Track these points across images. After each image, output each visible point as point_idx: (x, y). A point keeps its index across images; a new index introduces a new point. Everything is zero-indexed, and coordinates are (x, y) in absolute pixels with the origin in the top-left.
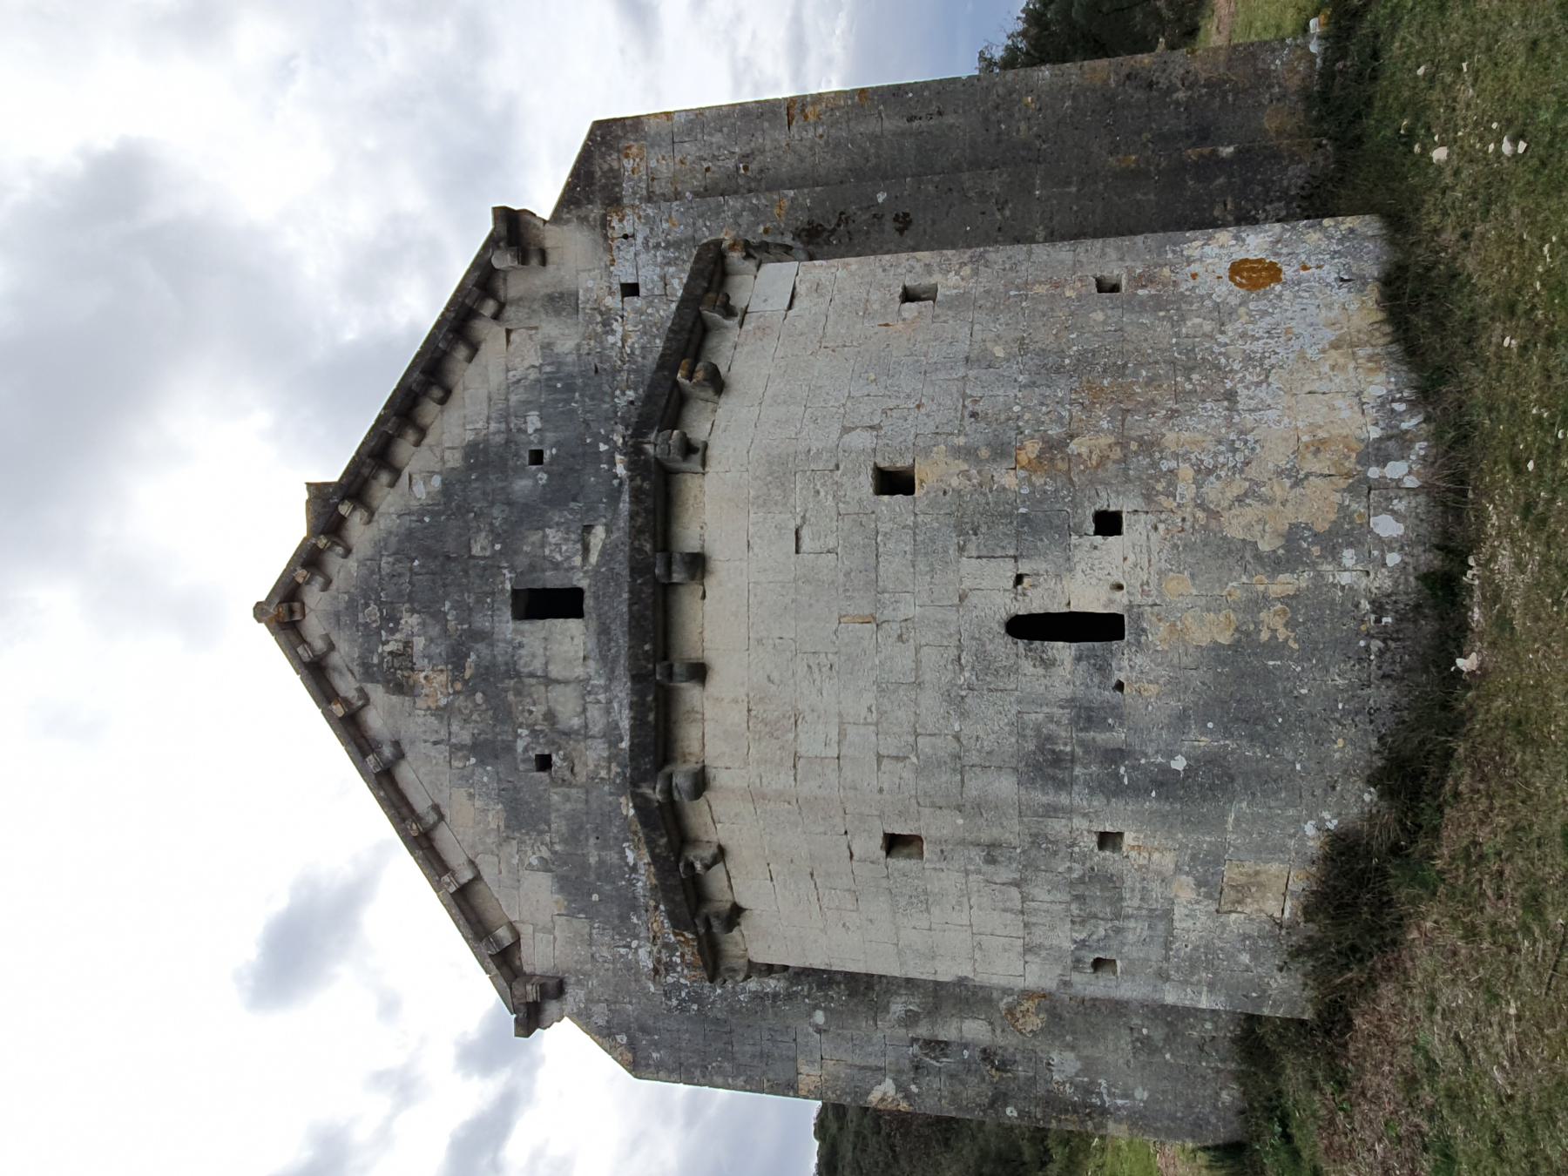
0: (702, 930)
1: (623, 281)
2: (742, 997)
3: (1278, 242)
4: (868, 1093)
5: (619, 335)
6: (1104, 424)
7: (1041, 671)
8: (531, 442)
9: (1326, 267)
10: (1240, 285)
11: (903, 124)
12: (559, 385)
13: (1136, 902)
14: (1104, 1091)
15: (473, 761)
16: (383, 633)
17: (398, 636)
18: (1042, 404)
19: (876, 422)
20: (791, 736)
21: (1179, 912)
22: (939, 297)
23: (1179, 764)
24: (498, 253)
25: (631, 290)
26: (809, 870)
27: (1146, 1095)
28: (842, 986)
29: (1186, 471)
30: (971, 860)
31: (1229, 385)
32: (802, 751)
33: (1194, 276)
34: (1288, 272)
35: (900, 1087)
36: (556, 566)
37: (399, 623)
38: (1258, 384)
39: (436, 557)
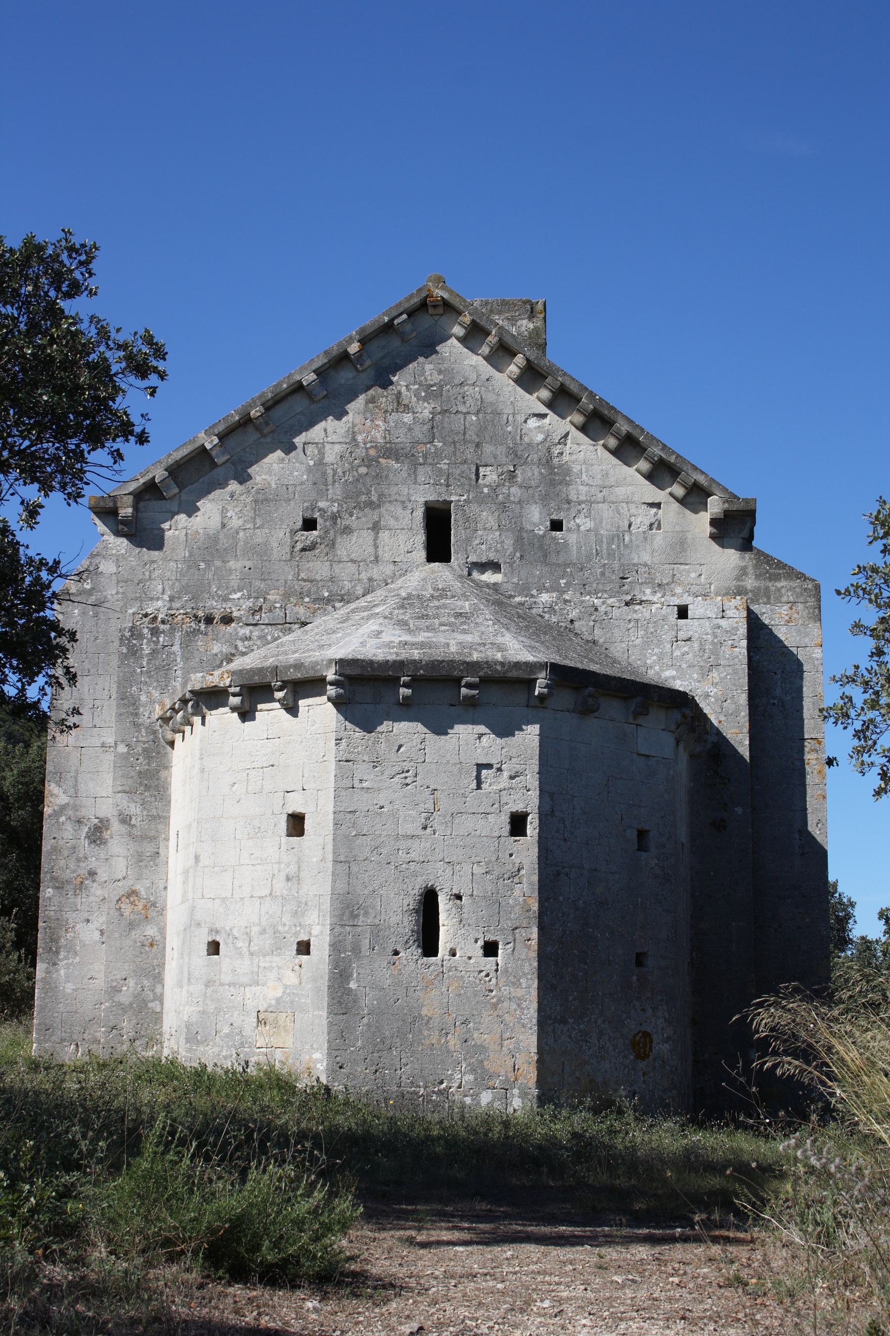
0: (232, 690)
1: (690, 607)
2: (134, 688)
3: (663, 1061)
5: (650, 598)
8: (569, 522)
9: (644, 1086)
10: (635, 1036)
12: (614, 547)
13: (262, 964)
14: (70, 961)
15: (311, 463)
16: (416, 387)
17: (414, 399)
18: (563, 913)
19: (557, 814)
20: (366, 758)
22: (640, 853)
23: (353, 985)
25: (683, 613)
26: (277, 764)
27: (69, 991)
28: (146, 767)
30: (288, 865)
31: (571, 1021)
33: (644, 1010)
34: (642, 1064)
35: (63, 808)
36: (468, 540)
37: (424, 401)
38: (570, 1037)
39: (478, 435)
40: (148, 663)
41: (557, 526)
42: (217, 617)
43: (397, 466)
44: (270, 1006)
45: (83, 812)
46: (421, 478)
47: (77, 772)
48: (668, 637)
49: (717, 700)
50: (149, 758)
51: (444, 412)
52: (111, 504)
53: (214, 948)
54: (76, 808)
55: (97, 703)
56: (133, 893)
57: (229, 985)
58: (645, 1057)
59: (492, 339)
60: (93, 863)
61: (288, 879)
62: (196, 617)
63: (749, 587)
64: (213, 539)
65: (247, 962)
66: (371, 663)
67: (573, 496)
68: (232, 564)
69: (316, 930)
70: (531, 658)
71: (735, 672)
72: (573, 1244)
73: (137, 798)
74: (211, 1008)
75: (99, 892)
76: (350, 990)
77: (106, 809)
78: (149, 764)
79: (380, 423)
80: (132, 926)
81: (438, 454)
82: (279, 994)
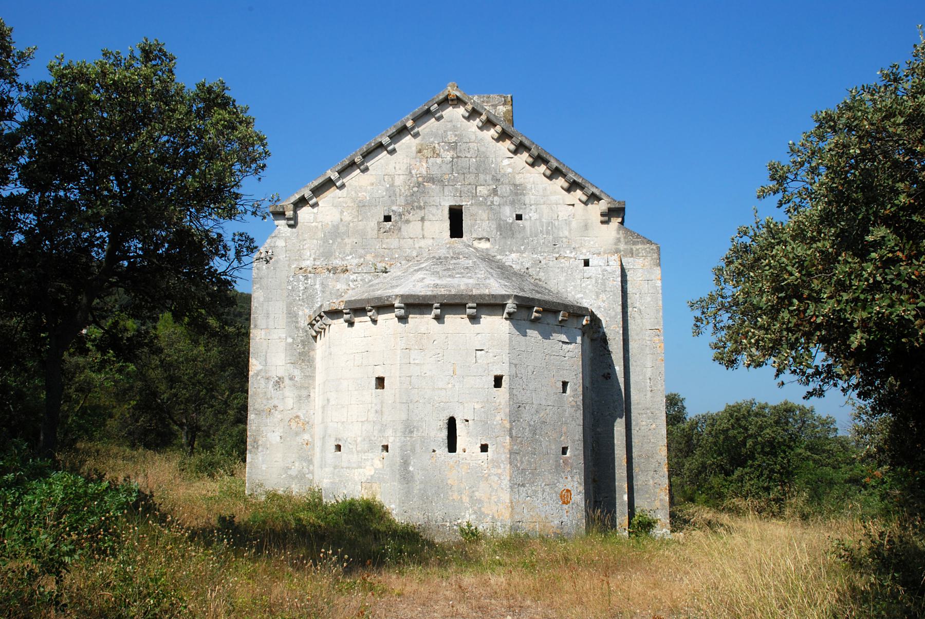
0: (344, 311)
4: (255, 358)
5: (569, 255)
6: (515, 447)
7: (439, 427)
11: (648, 376)
13: (363, 457)
15: (388, 186)
17: (442, 150)
21: (360, 470)
23: (411, 469)
24: (606, 203)
25: (586, 263)
29: (500, 471)
31: (527, 485)
32: (412, 351)
34: (565, 506)
36: (473, 226)
40: (303, 294)
41: (519, 217)
42: (340, 269)
43: (434, 187)
44: (368, 479)
45: (269, 374)
46: (446, 193)
47: (266, 352)
48: (578, 276)
49: (605, 309)
50: (304, 345)
51: (458, 157)
52: (281, 210)
53: (338, 448)
54: (266, 372)
55: (276, 316)
56: (297, 417)
57: (346, 468)
58: (568, 503)
59: (484, 117)
60: (276, 402)
61: (376, 412)
62: (328, 269)
63: (622, 249)
64: (336, 227)
65: (355, 456)
66: (418, 297)
67: (527, 202)
68: (347, 240)
69: (391, 439)
70: (504, 293)
71: (614, 294)
72: (626, 281)
73: (297, 366)
74: (337, 480)
75: (279, 416)
76: (410, 471)
77: (281, 372)
78: (304, 348)
79: (424, 164)
80: (297, 434)
81: (455, 180)
82: (372, 473)
